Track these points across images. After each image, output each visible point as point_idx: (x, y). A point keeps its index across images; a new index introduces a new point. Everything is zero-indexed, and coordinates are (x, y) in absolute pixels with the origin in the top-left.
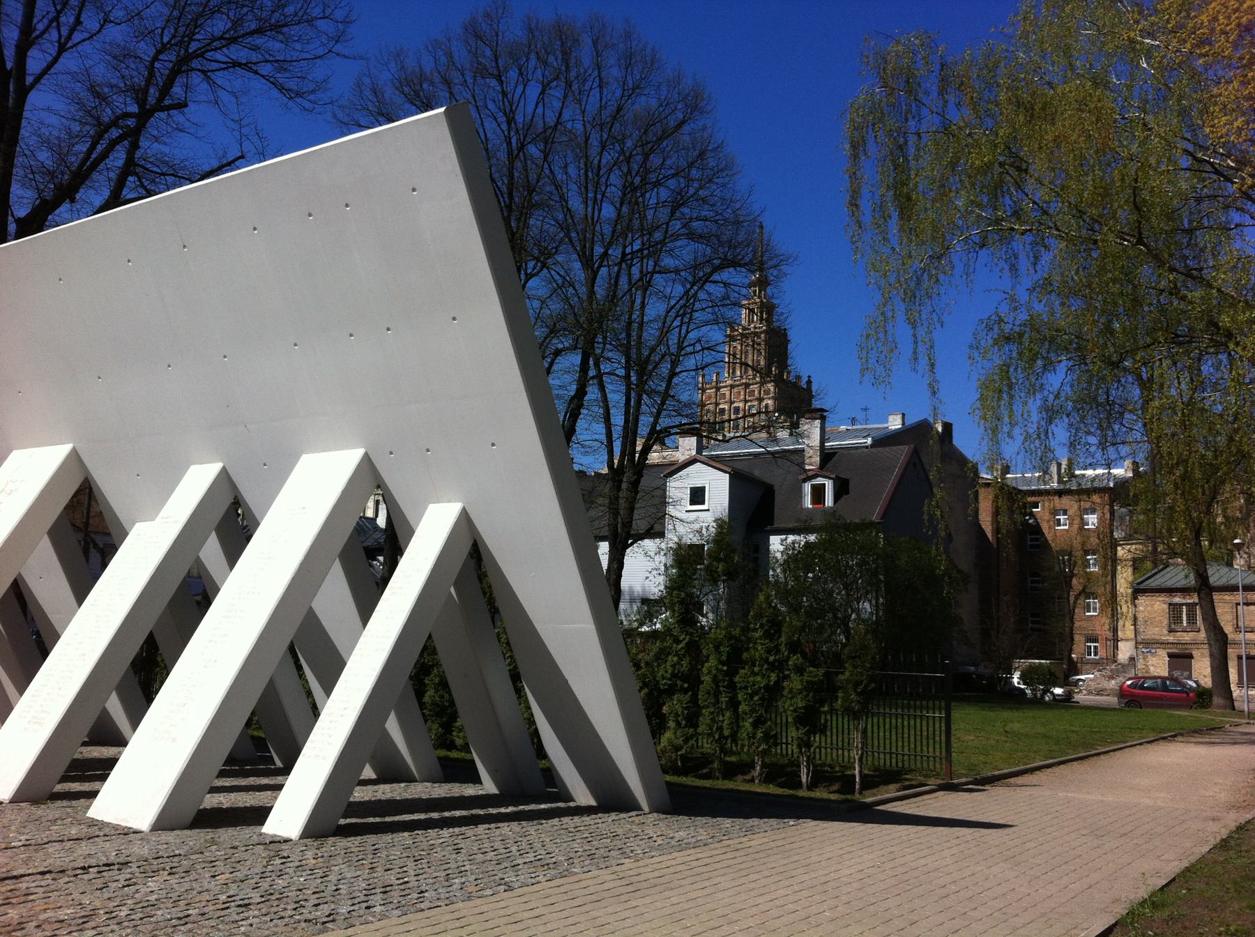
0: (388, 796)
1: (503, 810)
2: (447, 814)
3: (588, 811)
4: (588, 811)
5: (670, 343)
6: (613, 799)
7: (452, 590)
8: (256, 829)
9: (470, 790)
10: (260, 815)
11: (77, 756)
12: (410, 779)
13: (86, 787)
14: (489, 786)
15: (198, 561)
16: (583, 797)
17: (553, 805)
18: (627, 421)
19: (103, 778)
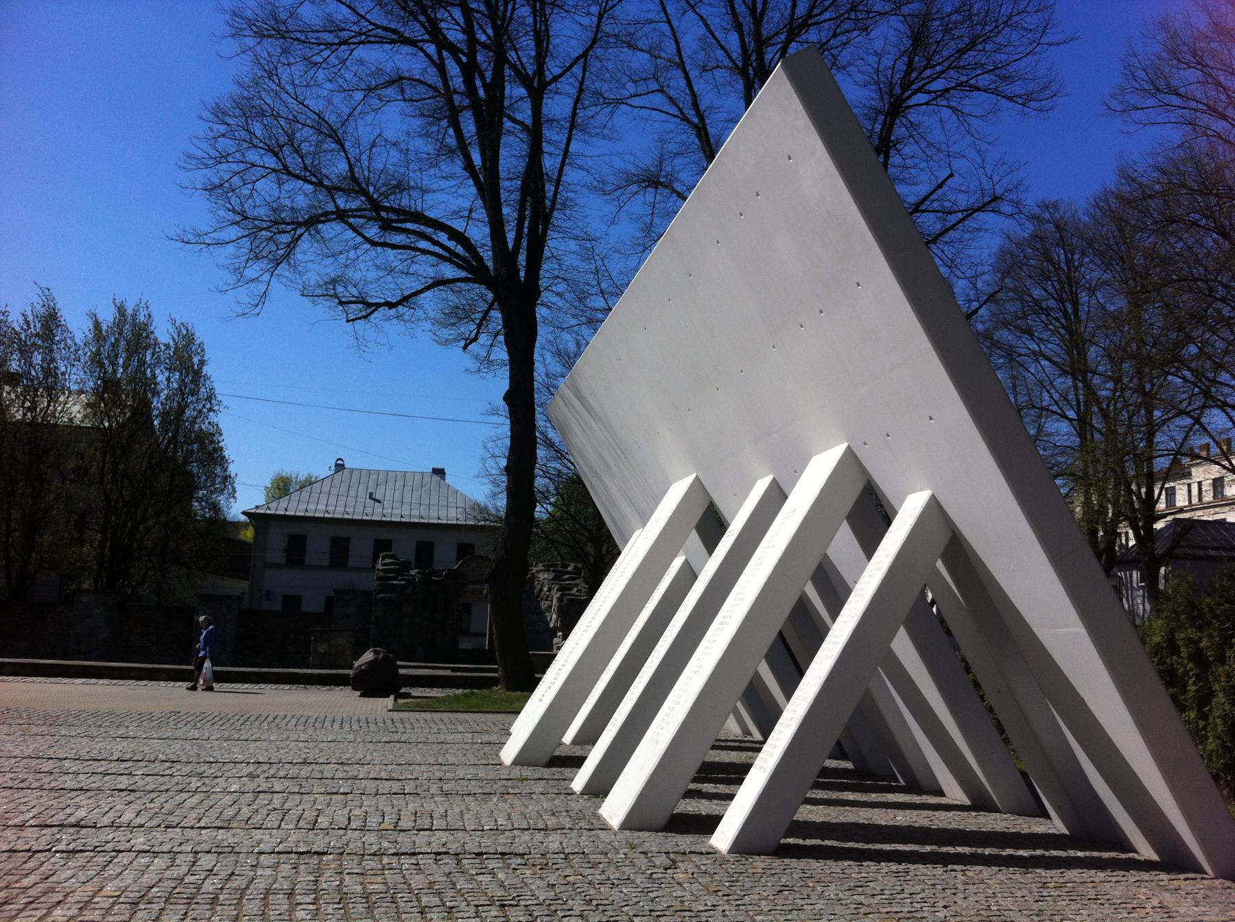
0: (953, 826)
1: (1021, 853)
2: (1038, 852)
3: (1147, 866)
4: (1147, 866)
5: (1221, 73)
6: (1174, 861)
7: (940, 565)
8: (701, 838)
9: (1038, 827)
10: (709, 824)
11: (707, 760)
12: (996, 810)
13: (722, 789)
14: (1057, 826)
15: (826, 557)
16: (1146, 851)
17: (870, 846)
18: (451, 262)
19: (740, 782)
